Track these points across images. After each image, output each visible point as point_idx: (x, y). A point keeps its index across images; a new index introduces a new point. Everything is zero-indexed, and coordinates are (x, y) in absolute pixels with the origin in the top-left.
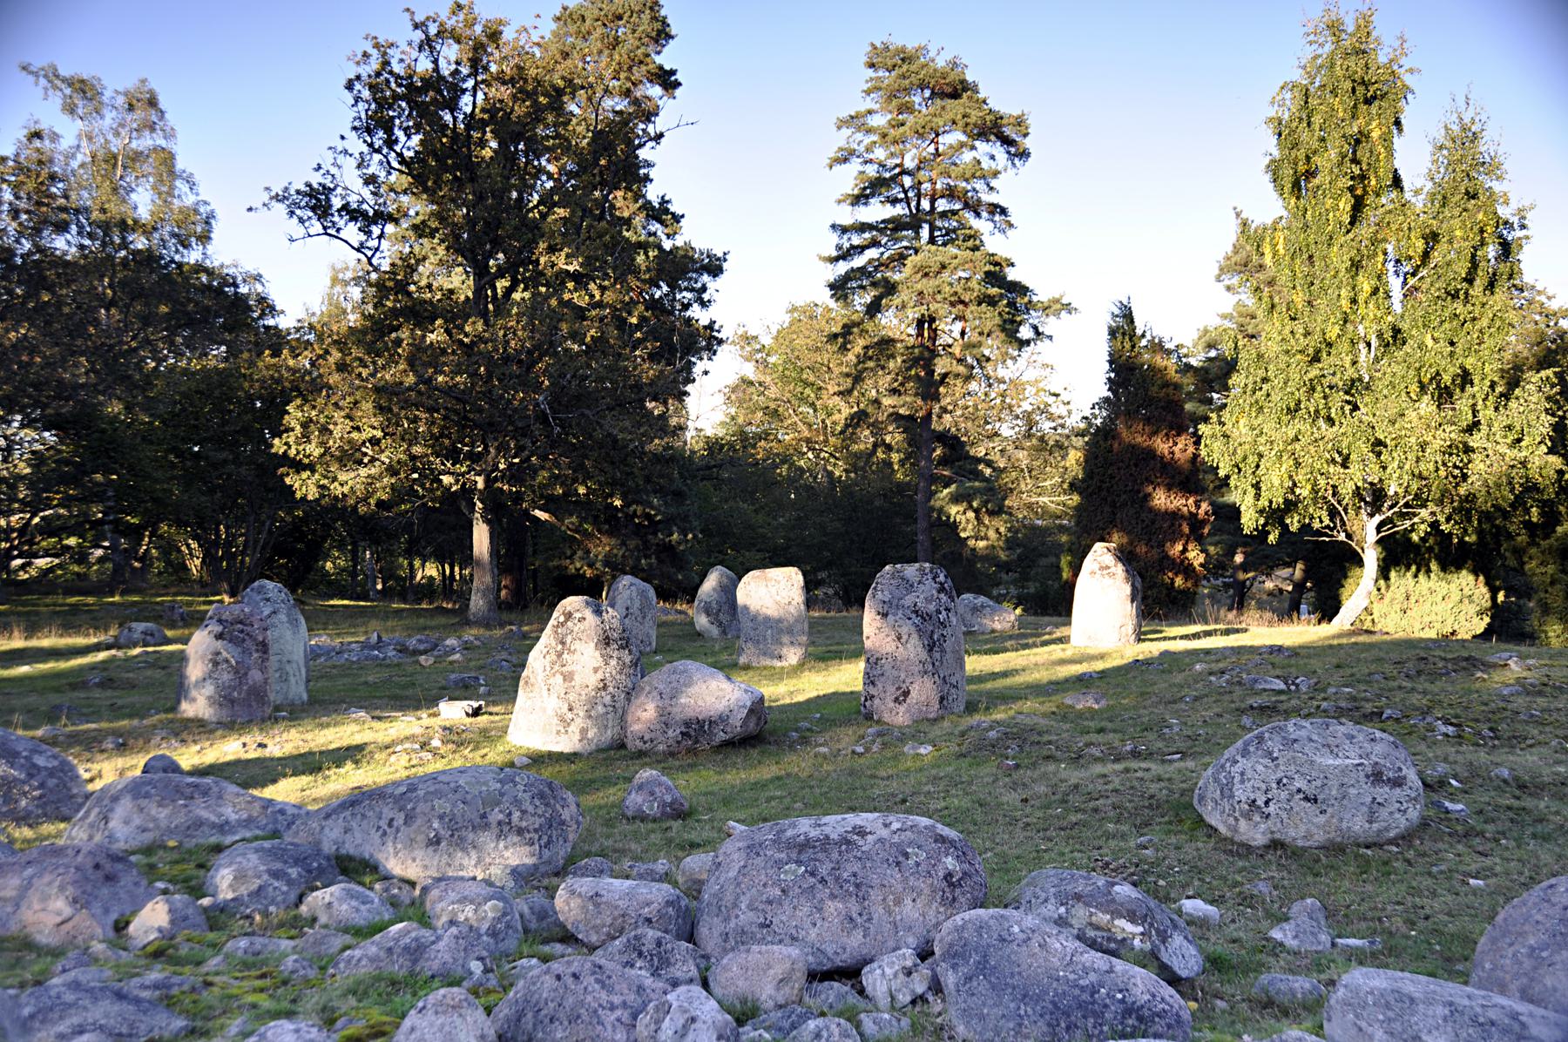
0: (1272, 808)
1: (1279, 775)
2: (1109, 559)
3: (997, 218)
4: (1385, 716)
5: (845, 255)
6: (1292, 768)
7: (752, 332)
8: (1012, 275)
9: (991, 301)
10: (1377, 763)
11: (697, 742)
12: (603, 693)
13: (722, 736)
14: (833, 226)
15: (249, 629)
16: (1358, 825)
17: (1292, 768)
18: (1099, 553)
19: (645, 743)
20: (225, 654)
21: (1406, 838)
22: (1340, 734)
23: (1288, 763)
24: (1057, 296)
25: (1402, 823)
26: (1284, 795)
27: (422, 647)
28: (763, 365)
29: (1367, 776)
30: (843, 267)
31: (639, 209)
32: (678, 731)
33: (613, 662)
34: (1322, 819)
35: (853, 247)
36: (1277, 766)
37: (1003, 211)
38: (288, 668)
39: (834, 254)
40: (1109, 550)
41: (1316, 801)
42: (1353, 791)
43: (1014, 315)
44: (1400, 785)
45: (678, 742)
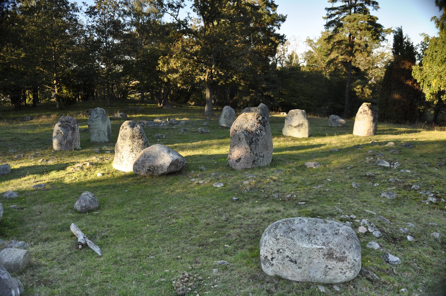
0: (274, 262)
1: (279, 247)
2: (367, 108)
3: (375, 5)
4: (412, 188)
5: (330, 16)
6: (285, 245)
7: (311, 39)
8: (378, 22)
9: (369, 29)
10: (331, 249)
11: (154, 173)
12: (132, 153)
13: (160, 172)
14: (326, 9)
15: (69, 124)
16: (318, 276)
17: (285, 245)
18: (364, 106)
19: (137, 172)
20: (61, 131)
21: (346, 284)
22: (320, 229)
23: (283, 243)
24: (390, 28)
25: (342, 278)
26: (280, 257)
27: (175, 123)
28: (315, 48)
29: (324, 255)
30: (329, 20)
31: (264, 4)
32: (147, 169)
33: (136, 143)
34: (299, 271)
35: (332, 14)
36: (278, 243)
37: (377, 3)
38: (100, 132)
39: (327, 16)
40: (367, 105)
41: (296, 263)
42: (316, 261)
43: (376, 33)
44: (342, 261)
45: (147, 173)
